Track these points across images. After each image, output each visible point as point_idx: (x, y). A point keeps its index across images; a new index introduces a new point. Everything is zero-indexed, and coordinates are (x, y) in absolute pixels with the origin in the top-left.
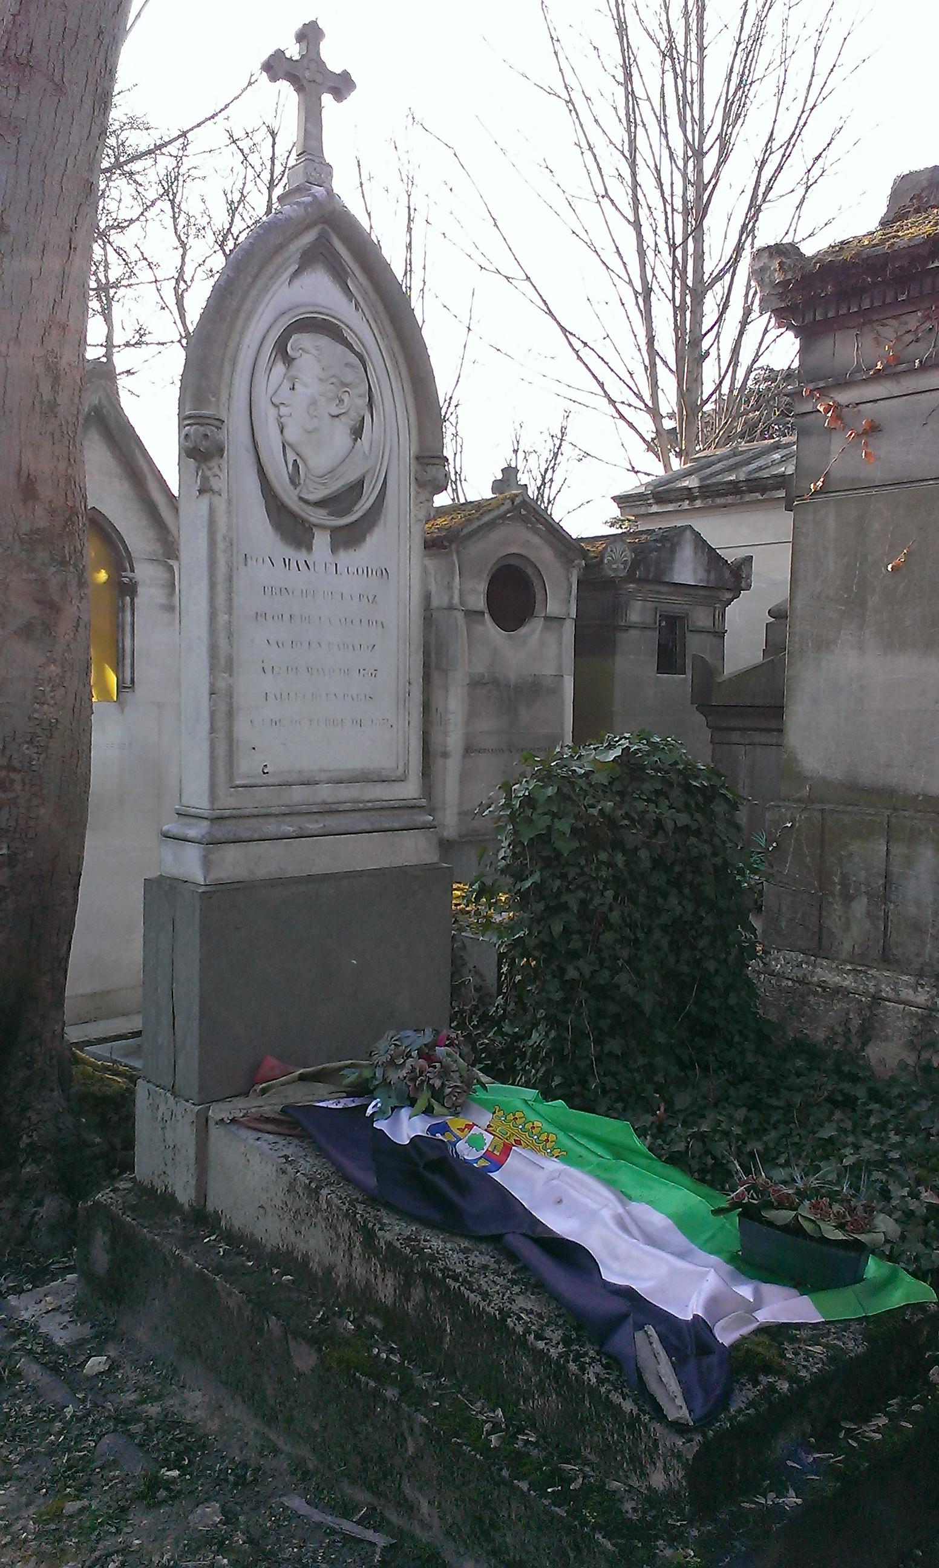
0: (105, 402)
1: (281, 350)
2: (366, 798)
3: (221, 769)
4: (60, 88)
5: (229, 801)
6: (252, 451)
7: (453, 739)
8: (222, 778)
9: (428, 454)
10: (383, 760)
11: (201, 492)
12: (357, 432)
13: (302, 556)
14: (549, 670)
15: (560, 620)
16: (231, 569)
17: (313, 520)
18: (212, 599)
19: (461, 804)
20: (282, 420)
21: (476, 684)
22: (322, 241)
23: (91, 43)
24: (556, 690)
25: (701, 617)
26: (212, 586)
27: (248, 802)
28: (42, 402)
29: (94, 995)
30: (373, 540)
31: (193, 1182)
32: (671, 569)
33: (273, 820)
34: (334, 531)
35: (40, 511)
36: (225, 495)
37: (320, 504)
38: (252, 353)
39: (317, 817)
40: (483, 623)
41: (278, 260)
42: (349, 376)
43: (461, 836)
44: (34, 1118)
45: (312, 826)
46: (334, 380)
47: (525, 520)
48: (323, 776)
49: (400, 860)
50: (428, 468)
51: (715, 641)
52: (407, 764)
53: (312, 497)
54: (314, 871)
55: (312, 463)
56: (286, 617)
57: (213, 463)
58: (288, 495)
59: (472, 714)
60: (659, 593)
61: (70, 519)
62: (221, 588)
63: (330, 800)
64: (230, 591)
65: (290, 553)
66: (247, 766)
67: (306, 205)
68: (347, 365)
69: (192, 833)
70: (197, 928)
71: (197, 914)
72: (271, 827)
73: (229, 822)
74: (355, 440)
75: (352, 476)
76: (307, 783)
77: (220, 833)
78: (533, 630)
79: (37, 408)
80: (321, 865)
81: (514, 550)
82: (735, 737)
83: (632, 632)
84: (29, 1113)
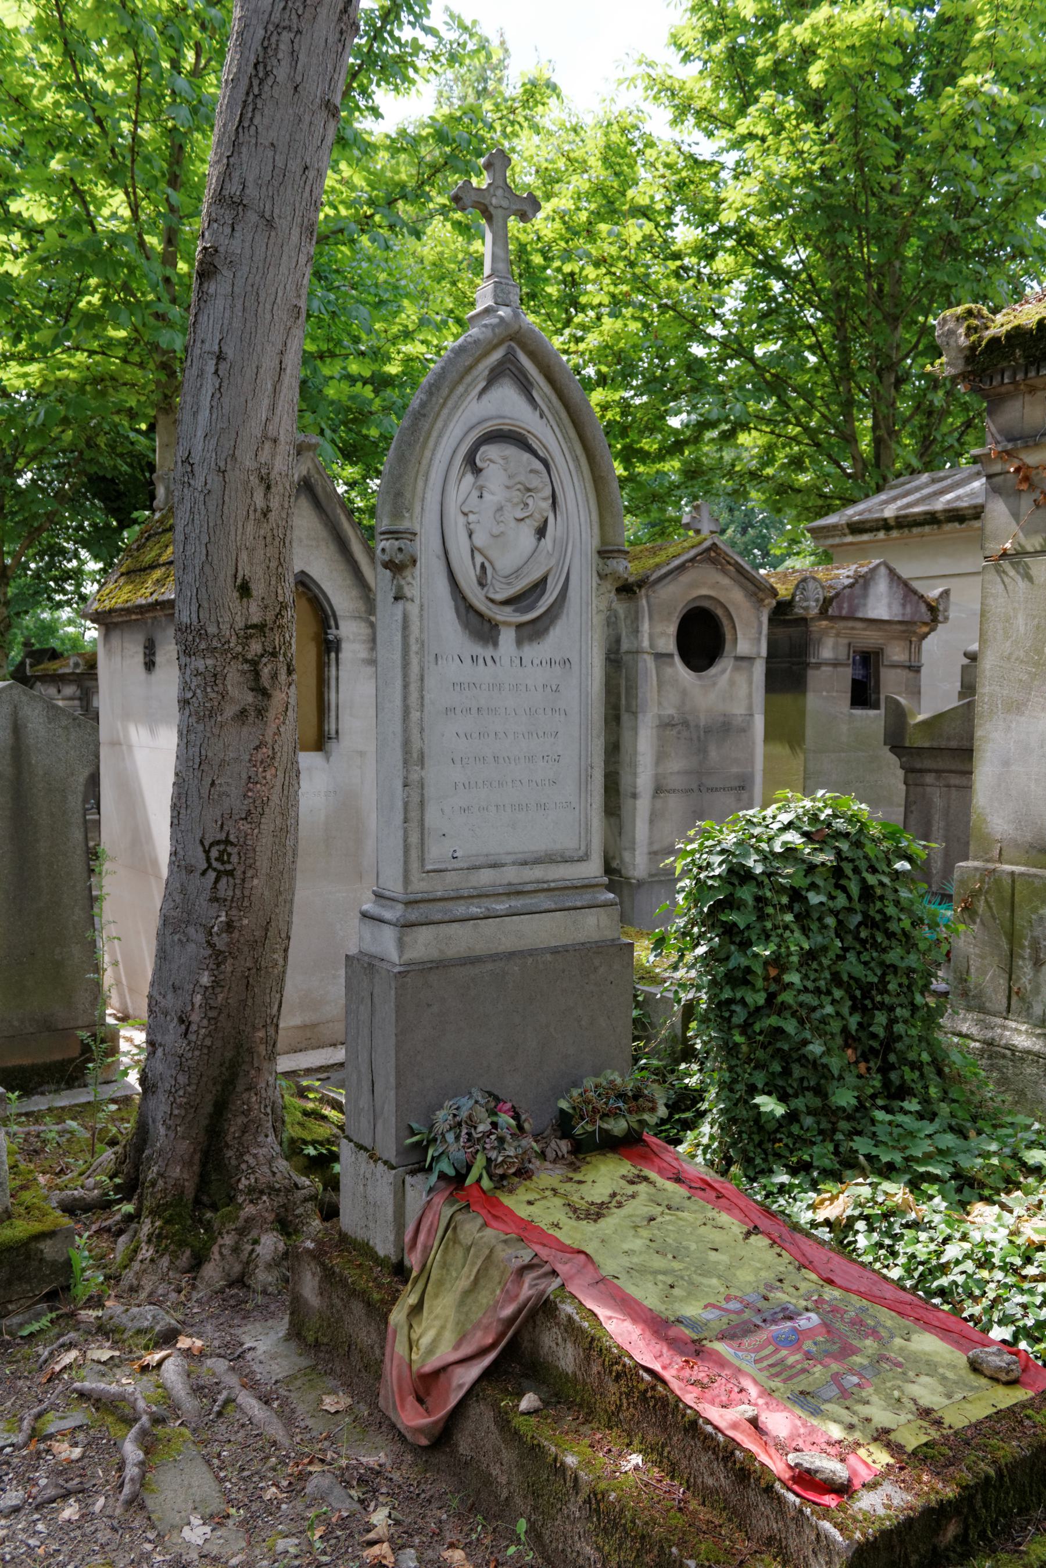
0: (313, 472)
1: (471, 463)
2: (550, 877)
3: (414, 854)
4: (270, 224)
5: (420, 885)
6: (443, 558)
7: (644, 779)
8: (415, 865)
9: (610, 548)
10: (567, 841)
11: (396, 599)
12: (541, 532)
13: (488, 652)
14: (738, 710)
15: (749, 659)
16: (422, 669)
17: (499, 618)
18: (405, 698)
19: (651, 843)
20: (471, 526)
21: (665, 725)
22: (510, 359)
23: (297, 178)
24: (745, 729)
25: (896, 653)
26: (406, 686)
27: (438, 887)
28: (255, 511)
29: (304, 1027)
30: (556, 633)
31: (392, 1238)
32: (865, 605)
33: (462, 902)
34: (519, 626)
35: (254, 608)
36: (417, 601)
37: (507, 602)
38: (443, 466)
39: (504, 898)
40: (672, 664)
41: (468, 379)
42: (534, 482)
43: (651, 875)
44: (252, 1162)
45: (501, 907)
46: (519, 486)
47: (713, 562)
48: (509, 859)
49: (581, 937)
50: (609, 562)
51: (912, 675)
52: (588, 846)
53: (499, 597)
54: (501, 949)
55: (498, 565)
56: (474, 711)
57: (407, 573)
58: (477, 597)
59: (661, 757)
60: (853, 628)
61: (279, 613)
62: (413, 688)
63: (515, 881)
64: (422, 689)
65: (478, 650)
66: (437, 852)
67: (493, 327)
68: (532, 471)
69: (388, 915)
70: (392, 1005)
71: (393, 992)
72: (460, 909)
73: (421, 905)
74: (539, 539)
75: (536, 575)
76: (494, 866)
77: (413, 915)
78: (723, 670)
79: (252, 517)
80: (508, 943)
81: (704, 592)
82: (929, 778)
83: (824, 668)
84: (246, 1158)
